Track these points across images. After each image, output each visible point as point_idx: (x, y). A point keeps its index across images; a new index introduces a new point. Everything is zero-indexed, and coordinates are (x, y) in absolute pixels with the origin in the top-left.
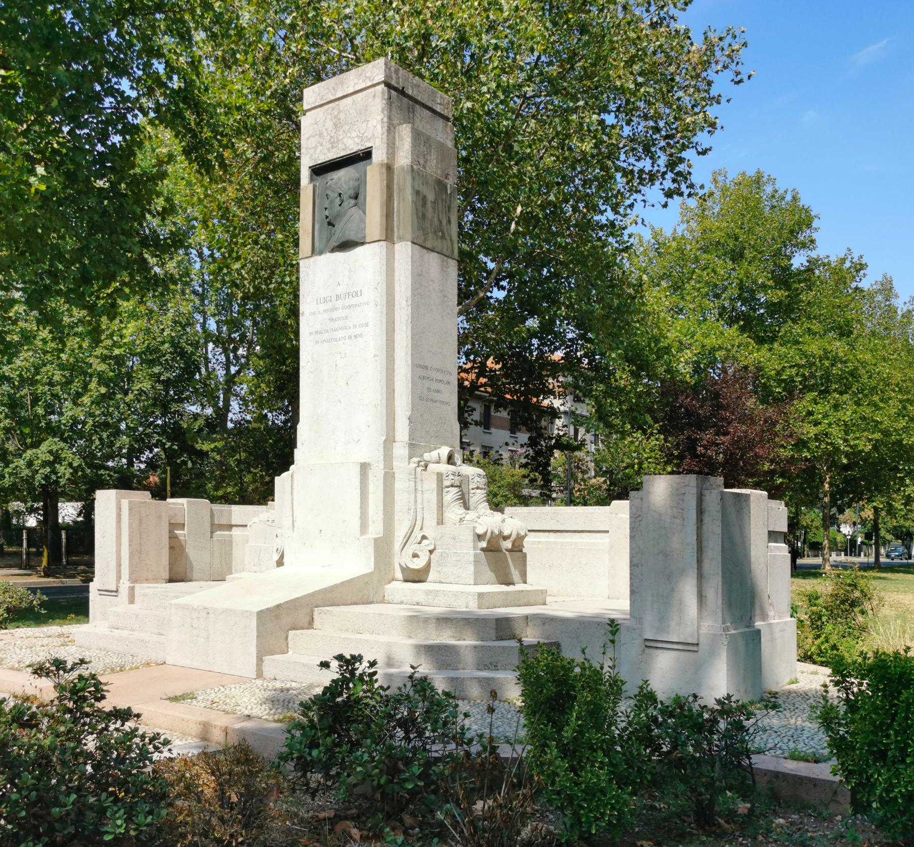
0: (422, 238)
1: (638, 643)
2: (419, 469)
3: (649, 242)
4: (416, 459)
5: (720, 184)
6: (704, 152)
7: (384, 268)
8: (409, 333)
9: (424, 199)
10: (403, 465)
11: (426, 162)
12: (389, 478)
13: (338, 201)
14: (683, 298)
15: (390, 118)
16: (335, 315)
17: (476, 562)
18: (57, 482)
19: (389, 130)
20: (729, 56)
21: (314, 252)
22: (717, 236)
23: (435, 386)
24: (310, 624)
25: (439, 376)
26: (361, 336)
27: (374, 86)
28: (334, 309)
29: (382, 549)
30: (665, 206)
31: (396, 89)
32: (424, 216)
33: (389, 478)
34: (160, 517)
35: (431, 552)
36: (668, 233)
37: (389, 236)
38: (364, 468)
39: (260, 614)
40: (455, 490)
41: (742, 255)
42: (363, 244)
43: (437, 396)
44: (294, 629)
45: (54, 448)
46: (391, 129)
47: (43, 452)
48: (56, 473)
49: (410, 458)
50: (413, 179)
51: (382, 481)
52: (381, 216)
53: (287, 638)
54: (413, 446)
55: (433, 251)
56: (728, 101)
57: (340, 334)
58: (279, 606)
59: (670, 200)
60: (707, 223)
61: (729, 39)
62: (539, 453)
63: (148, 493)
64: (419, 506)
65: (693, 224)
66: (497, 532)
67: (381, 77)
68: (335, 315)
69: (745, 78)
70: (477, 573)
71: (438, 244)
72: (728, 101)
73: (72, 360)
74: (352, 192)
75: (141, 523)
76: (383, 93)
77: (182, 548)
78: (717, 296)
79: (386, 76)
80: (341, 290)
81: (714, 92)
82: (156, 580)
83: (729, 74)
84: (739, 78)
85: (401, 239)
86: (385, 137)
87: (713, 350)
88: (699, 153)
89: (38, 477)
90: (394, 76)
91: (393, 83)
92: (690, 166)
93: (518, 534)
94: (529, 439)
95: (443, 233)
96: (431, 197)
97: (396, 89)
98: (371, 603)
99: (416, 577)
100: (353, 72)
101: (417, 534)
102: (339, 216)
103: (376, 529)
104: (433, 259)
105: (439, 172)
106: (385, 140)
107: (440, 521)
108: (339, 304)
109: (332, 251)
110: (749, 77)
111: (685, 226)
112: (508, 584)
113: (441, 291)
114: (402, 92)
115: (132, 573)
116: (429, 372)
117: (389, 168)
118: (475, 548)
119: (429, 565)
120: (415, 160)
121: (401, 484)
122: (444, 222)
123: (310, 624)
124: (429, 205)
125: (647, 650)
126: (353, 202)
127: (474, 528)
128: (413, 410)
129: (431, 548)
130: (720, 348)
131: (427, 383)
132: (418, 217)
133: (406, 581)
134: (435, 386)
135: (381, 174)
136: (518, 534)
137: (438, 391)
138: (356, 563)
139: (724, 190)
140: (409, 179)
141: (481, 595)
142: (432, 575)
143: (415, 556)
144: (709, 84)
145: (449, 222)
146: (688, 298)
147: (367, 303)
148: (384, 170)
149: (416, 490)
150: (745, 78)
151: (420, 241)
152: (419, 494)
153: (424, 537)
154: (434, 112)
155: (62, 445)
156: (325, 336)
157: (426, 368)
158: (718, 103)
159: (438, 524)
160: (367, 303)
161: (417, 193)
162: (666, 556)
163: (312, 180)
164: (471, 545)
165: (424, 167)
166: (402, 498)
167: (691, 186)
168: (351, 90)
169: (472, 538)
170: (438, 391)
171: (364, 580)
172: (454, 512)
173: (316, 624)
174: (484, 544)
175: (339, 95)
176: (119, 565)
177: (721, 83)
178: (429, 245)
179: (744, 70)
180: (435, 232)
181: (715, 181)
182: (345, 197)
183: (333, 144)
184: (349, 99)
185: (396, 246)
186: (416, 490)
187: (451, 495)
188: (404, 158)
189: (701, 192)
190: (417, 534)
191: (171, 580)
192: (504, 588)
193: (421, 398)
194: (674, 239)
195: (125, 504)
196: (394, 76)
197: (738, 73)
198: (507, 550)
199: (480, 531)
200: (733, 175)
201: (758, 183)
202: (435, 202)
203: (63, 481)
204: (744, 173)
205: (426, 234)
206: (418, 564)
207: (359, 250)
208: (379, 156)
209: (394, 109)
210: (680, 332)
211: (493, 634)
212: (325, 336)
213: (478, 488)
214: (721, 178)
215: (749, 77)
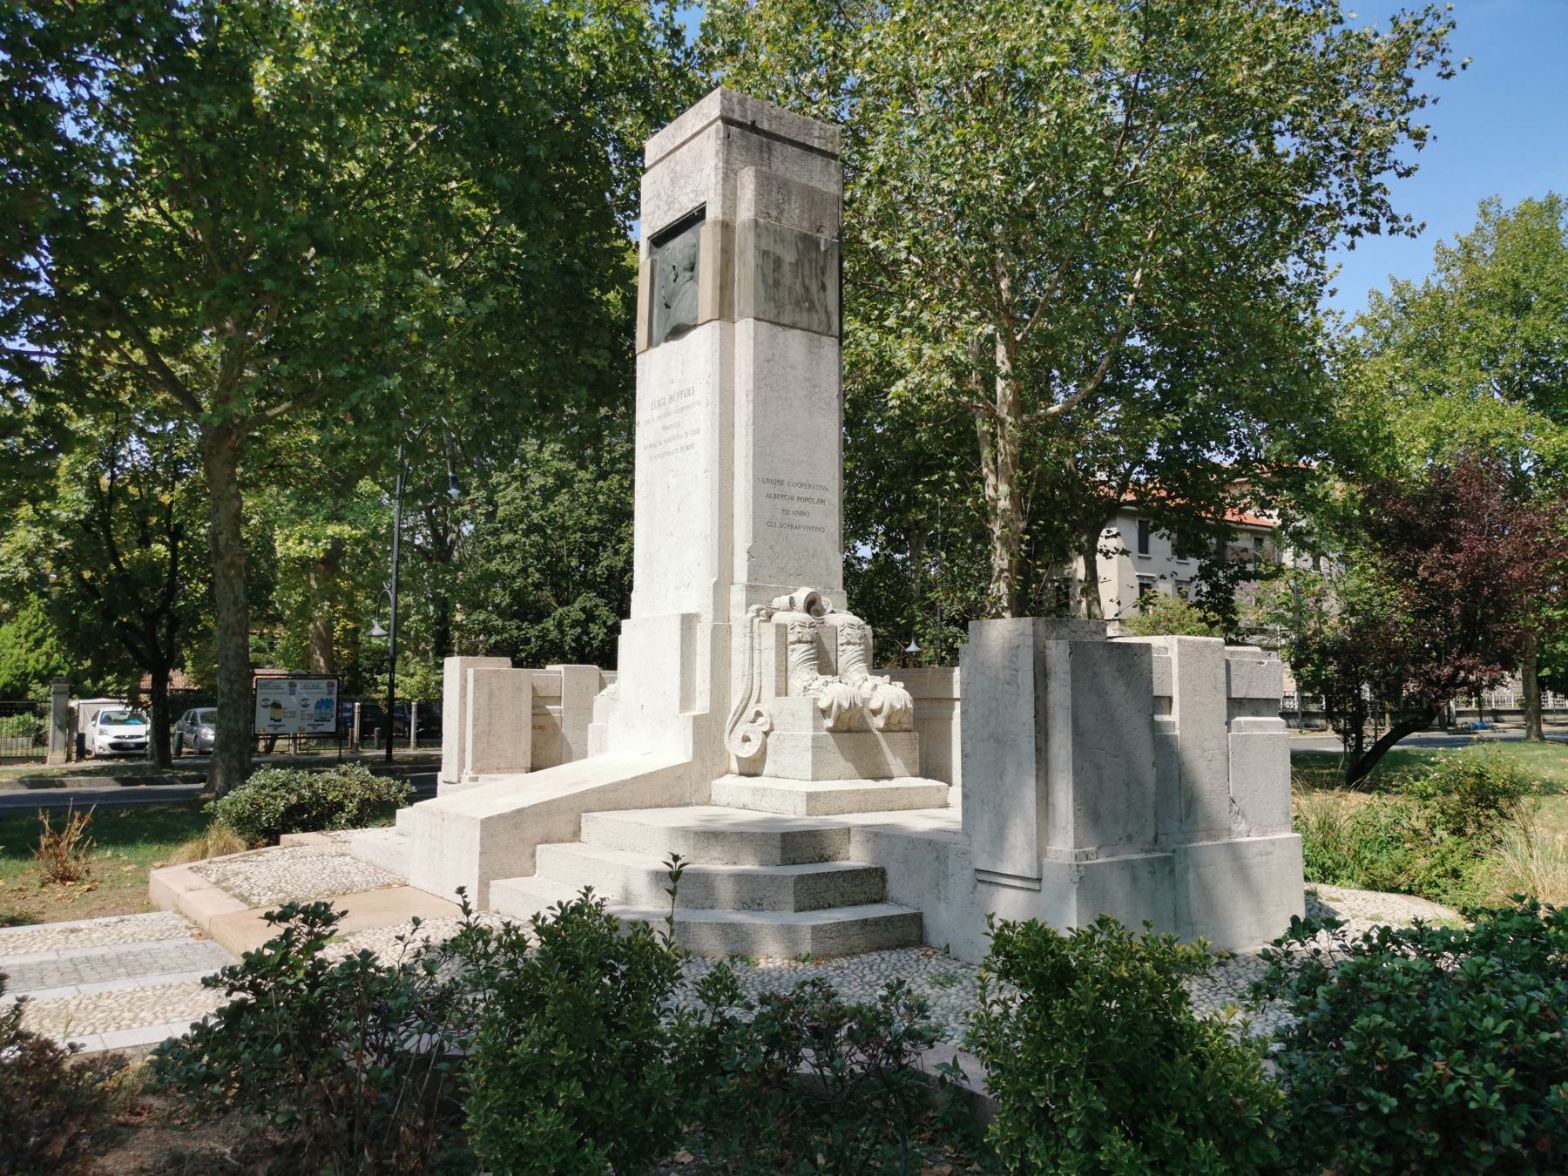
0: (774, 312)
1: (968, 873)
2: (756, 620)
3: (1391, 300)
4: (755, 607)
5: (1492, 217)
6: (1408, 173)
7: (717, 355)
8: (750, 438)
9: (778, 263)
10: (739, 615)
11: (781, 212)
12: (721, 635)
13: (672, 276)
14: (1444, 371)
15: (727, 162)
16: (669, 421)
17: (817, 746)
18: (589, 643)
19: (726, 178)
20: (1430, 43)
21: (651, 343)
22: (1490, 285)
23: (797, 506)
24: (576, 836)
25: (804, 493)
26: (692, 446)
27: (710, 124)
28: (667, 414)
29: (707, 733)
30: (1352, 246)
31: (740, 125)
32: (777, 284)
33: (721, 635)
34: (519, 689)
35: (766, 734)
36: (1418, 285)
37: (725, 312)
38: (688, 621)
39: (487, 824)
40: (804, 647)
41: (1528, 307)
42: (695, 326)
43: (803, 520)
44: (547, 841)
45: (588, 604)
46: (729, 175)
47: (575, 611)
48: (588, 634)
49: (748, 605)
50: (758, 236)
51: (709, 637)
52: (714, 288)
53: (533, 855)
54: (752, 589)
55: (793, 327)
56: (1435, 102)
57: (673, 446)
58: (520, 811)
59: (1357, 238)
60: (1474, 270)
61: (1429, 21)
62: (1215, 587)
63: (507, 660)
64: (756, 671)
65: (1456, 272)
66: (846, 705)
67: (716, 113)
68: (669, 421)
69: (1457, 68)
70: (816, 764)
71: (803, 318)
72: (1435, 102)
73: (611, 502)
74: (686, 263)
75: (491, 696)
76: (717, 131)
77: (556, 728)
78: (1493, 363)
79: (723, 109)
80: (674, 389)
81: (1413, 93)
82: (511, 769)
83: (1434, 67)
84: (1449, 69)
85: (742, 316)
86: (719, 187)
87: (1485, 439)
88: (1400, 175)
89: (568, 639)
90: (737, 108)
91: (737, 117)
92: (1385, 192)
93: (892, 707)
94: (1200, 568)
95: (812, 303)
96: (789, 257)
97: (740, 125)
98: (687, 805)
99: (751, 769)
100: (691, 112)
101: (750, 713)
102: (673, 294)
103: (702, 705)
104: (795, 342)
105: (805, 224)
106: (720, 191)
107: (782, 690)
108: (672, 407)
109: (666, 340)
110: (1464, 66)
111: (1442, 276)
112: (876, 779)
113: (808, 380)
114: (753, 128)
115: (475, 762)
116: (786, 488)
117: (726, 227)
118: (815, 728)
119: (763, 750)
120: (763, 208)
121: (738, 641)
122: (814, 288)
123: (576, 836)
124: (786, 269)
125: (981, 887)
126: (688, 274)
127: (815, 700)
128: (755, 539)
129: (766, 728)
130: (1498, 434)
131: (781, 503)
132: (766, 285)
133: (741, 774)
134: (797, 506)
135: (714, 234)
136: (892, 707)
137: (802, 513)
138: (674, 749)
139: (1502, 227)
140: (751, 237)
141: (812, 797)
142: (769, 767)
143: (746, 739)
144: (1409, 83)
145: (823, 287)
146: (1451, 369)
147: (699, 403)
148: (718, 229)
149: (752, 648)
150: (1457, 68)
151: (772, 317)
152: (756, 654)
153: (758, 714)
154: (810, 149)
155: (600, 601)
156: (659, 450)
157: (781, 482)
158: (1422, 106)
159: (778, 694)
160: (699, 403)
161: (765, 254)
162: (999, 742)
163: (651, 253)
164: (810, 723)
165: (778, 220)
166: (738, 659)
167: (1394, 219)
168: (689, 134)
169: (811, 714)
170: (802, 513)
171: (674, 775)
172: (802, 676)
173: (584, 835)
174: (829, 723)
175: (678, 142)
176: (462, 750)
177: (1424, 80)
178: (786, 319)
179: (1455, 61)
180: (798, 303)
181: (1485, 213)
182: (679, 269)
183: (670, 204)
184: (685, 147)
185: (738, 325)
186: (752, 648)
187: (798, 654)
188: (746, 212)
189: (1407, 225)
190: (750, 713)
191: (533, 769)
192: (870, 784)
193: (770, 524)
194: (1426, 294)
195: (470, 672)
196: (737, 108)
197: (1445, 64)
198: (881, 730)
199: (823, 704)
200: (1511, 203)
201: (1551, 210)
202: (797, 265)
203: (596, 643)
204: (1530, 200)
205: (779, 306)
206: (750, 750)
207: (692, 335)
208: (713, 213)
209: (735, 149)
210: (1435, 415)
211: (777, 854)
212: (659, 450)
213: (849, 643)
214: (1492, 209)
215: (1464, 66)
